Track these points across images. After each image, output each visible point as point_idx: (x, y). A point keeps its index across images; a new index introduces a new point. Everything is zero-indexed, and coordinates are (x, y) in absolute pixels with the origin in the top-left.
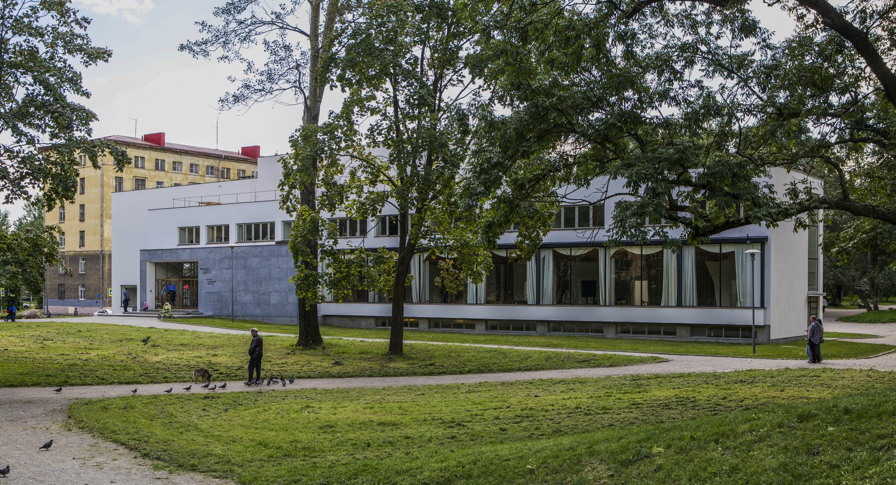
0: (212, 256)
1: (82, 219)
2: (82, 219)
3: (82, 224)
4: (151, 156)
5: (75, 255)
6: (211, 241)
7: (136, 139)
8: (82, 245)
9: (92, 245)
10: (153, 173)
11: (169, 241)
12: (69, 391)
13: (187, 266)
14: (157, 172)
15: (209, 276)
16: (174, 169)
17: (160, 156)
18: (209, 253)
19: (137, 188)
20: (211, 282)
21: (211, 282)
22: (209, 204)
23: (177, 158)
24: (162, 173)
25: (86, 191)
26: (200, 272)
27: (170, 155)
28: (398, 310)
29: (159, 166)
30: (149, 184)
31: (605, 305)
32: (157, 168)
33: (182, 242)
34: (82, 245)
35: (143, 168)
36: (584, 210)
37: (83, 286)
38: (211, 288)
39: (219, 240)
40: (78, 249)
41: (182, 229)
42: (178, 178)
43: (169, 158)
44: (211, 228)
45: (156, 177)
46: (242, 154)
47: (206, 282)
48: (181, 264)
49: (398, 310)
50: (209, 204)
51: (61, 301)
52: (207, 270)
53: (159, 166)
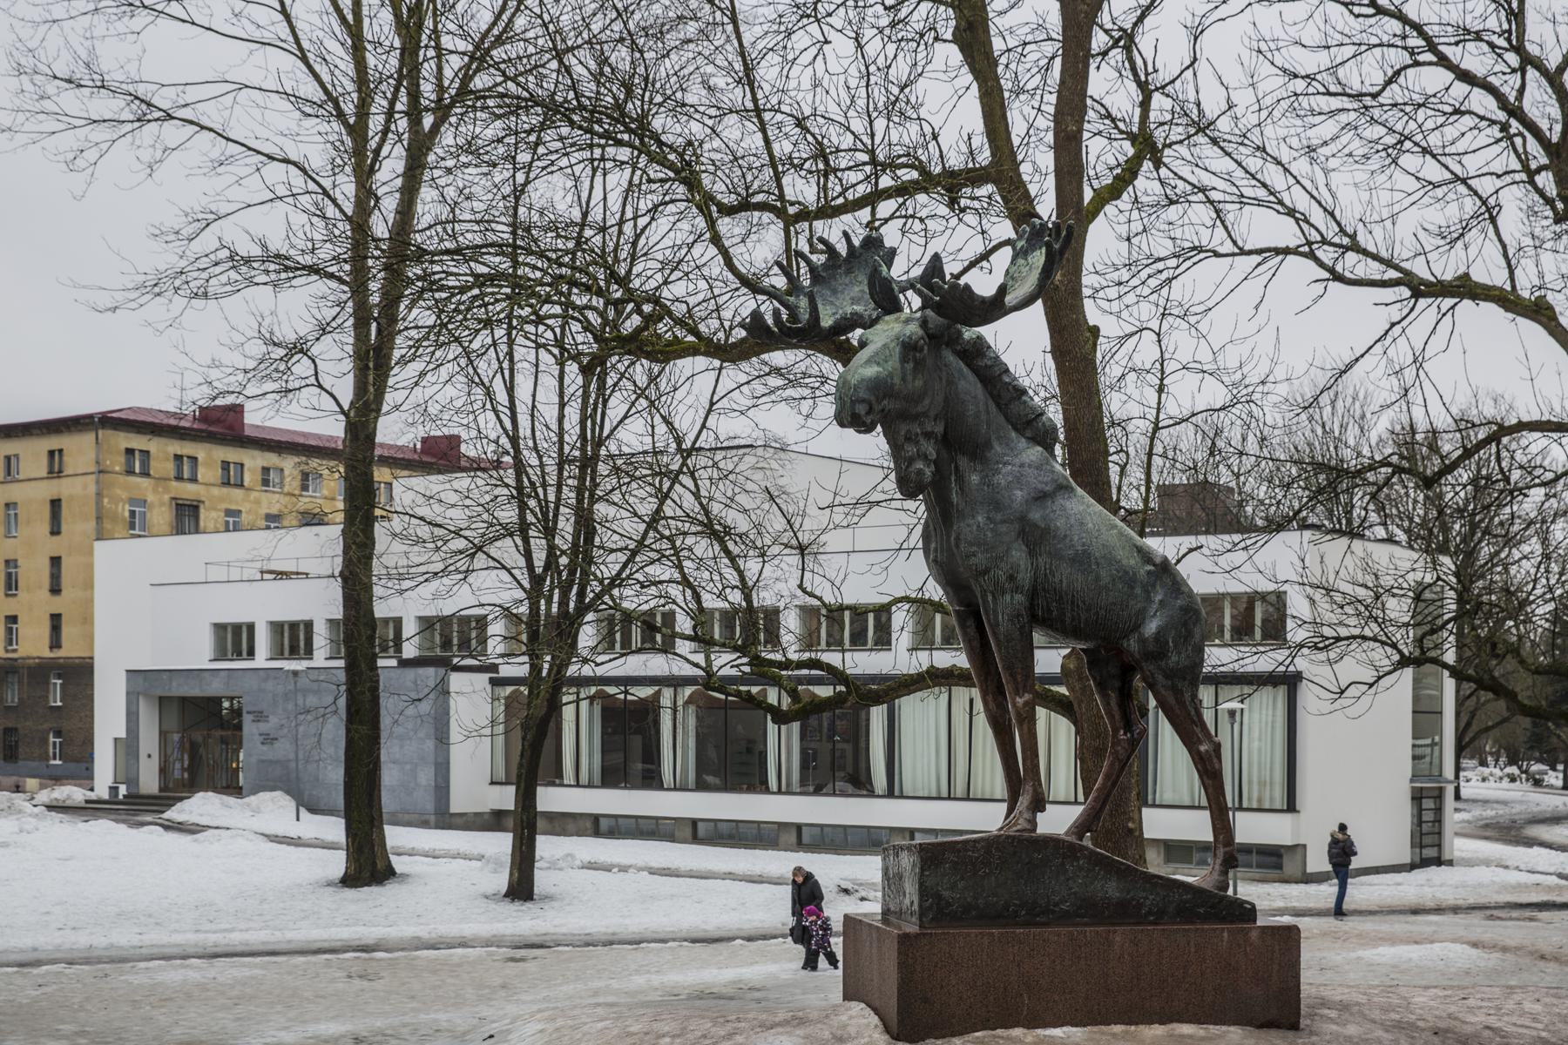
0: (269, 685)
1: (55, 590)
2: (55, 590)
3: (56, 599)
4: (210, 456)
5: (40, 666)
6: (278, 653)
7: (182, 417)
8: (56, 643)
9: (70, 649)
10: (216, 491)
11: (197, 653)
12: (1365, 889)
13: (226, 704)
14: (225, 490)
15: (263, 727)
16: (266, 482)
17: (232, 454)
18: (266, 680)
19: (179, 530)
20: (268, 739)
21: (268, 739)
22: (281, 575)
23: (271, 459)
24: (237, 493)
25: (64, 528)
26: (247, 720)
27: (256, 453)
28: (526, 797)
29: (231, 477)
30: (207, 517)
31: (780, 792)
32: (226, 483)
33: (221, 655)
34: (56, 643)
35: (194, 480)
36: (859, 612)
37: (58, 734)
38: (268, 752)
39: (294, 652)
40: (47, 653)
41: (220, 628)
42: (272, 502)
43: (253, 461)
44: (277, 627)
45: (222, 499)
46: (423, 451)
47: (258, 739)
48: (217, 701)
49: (526, 797)
50: (281, 575)
51: (10, 767)
52: (260, 716)
53: (231, 477)
